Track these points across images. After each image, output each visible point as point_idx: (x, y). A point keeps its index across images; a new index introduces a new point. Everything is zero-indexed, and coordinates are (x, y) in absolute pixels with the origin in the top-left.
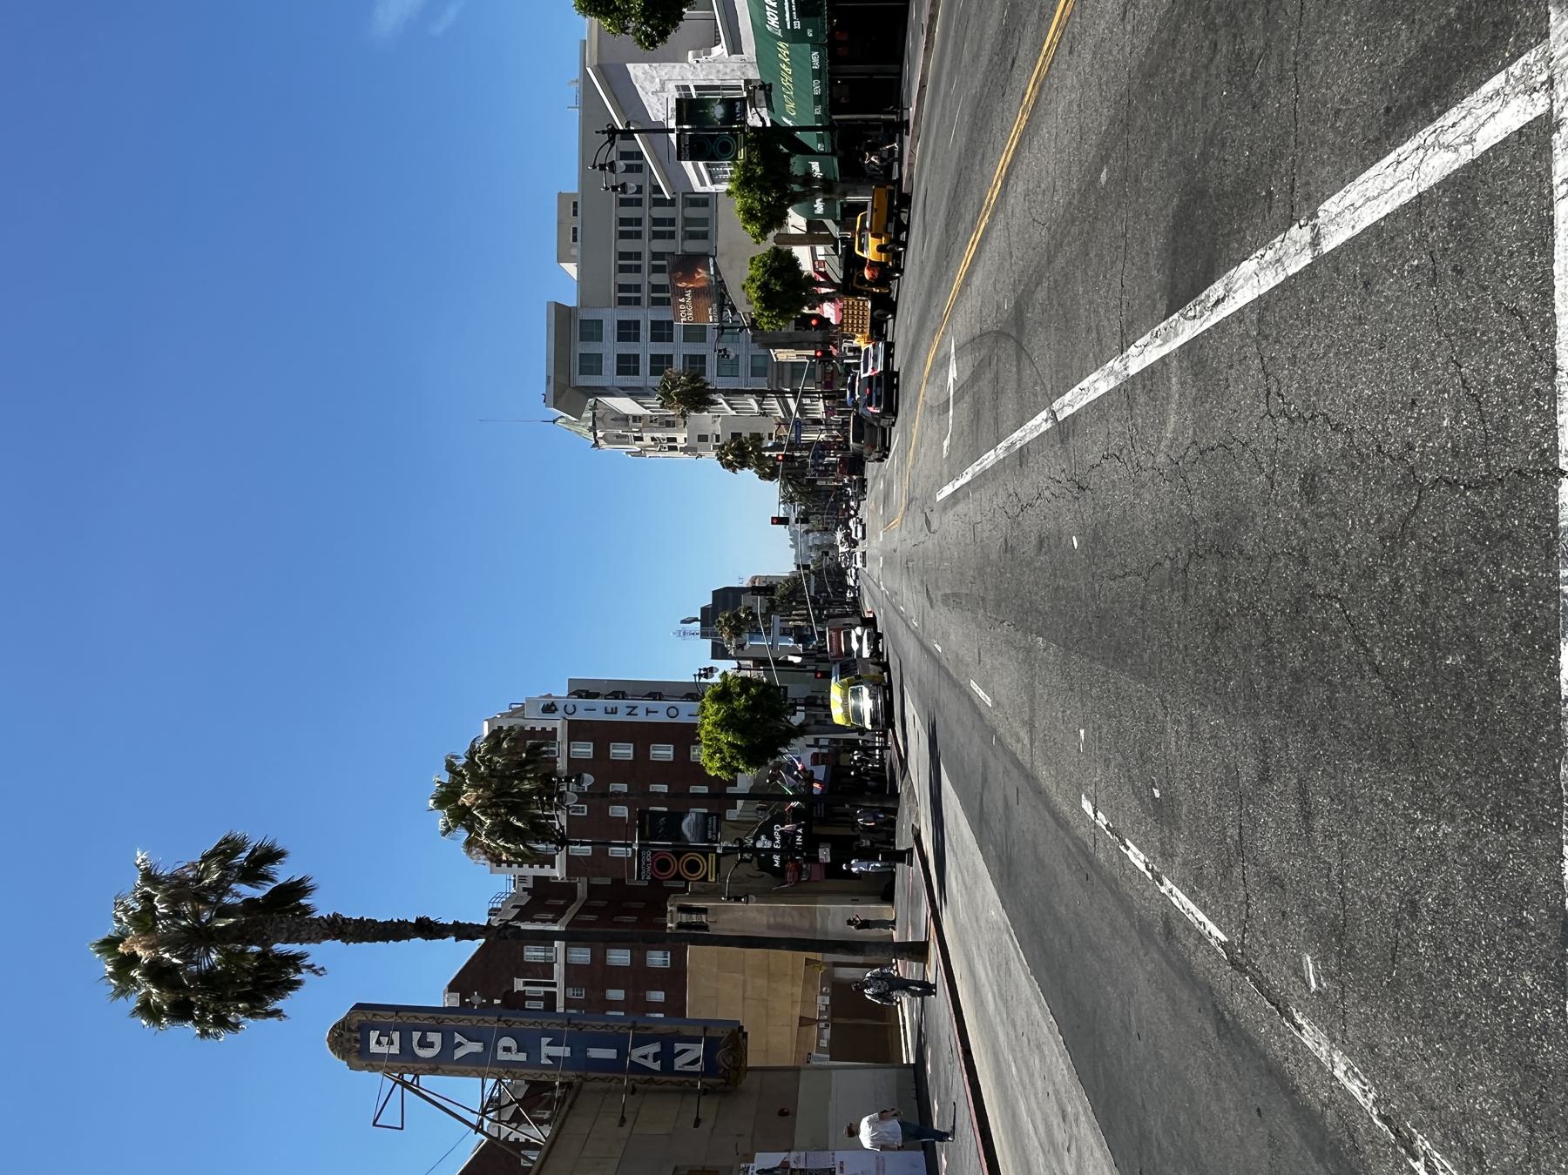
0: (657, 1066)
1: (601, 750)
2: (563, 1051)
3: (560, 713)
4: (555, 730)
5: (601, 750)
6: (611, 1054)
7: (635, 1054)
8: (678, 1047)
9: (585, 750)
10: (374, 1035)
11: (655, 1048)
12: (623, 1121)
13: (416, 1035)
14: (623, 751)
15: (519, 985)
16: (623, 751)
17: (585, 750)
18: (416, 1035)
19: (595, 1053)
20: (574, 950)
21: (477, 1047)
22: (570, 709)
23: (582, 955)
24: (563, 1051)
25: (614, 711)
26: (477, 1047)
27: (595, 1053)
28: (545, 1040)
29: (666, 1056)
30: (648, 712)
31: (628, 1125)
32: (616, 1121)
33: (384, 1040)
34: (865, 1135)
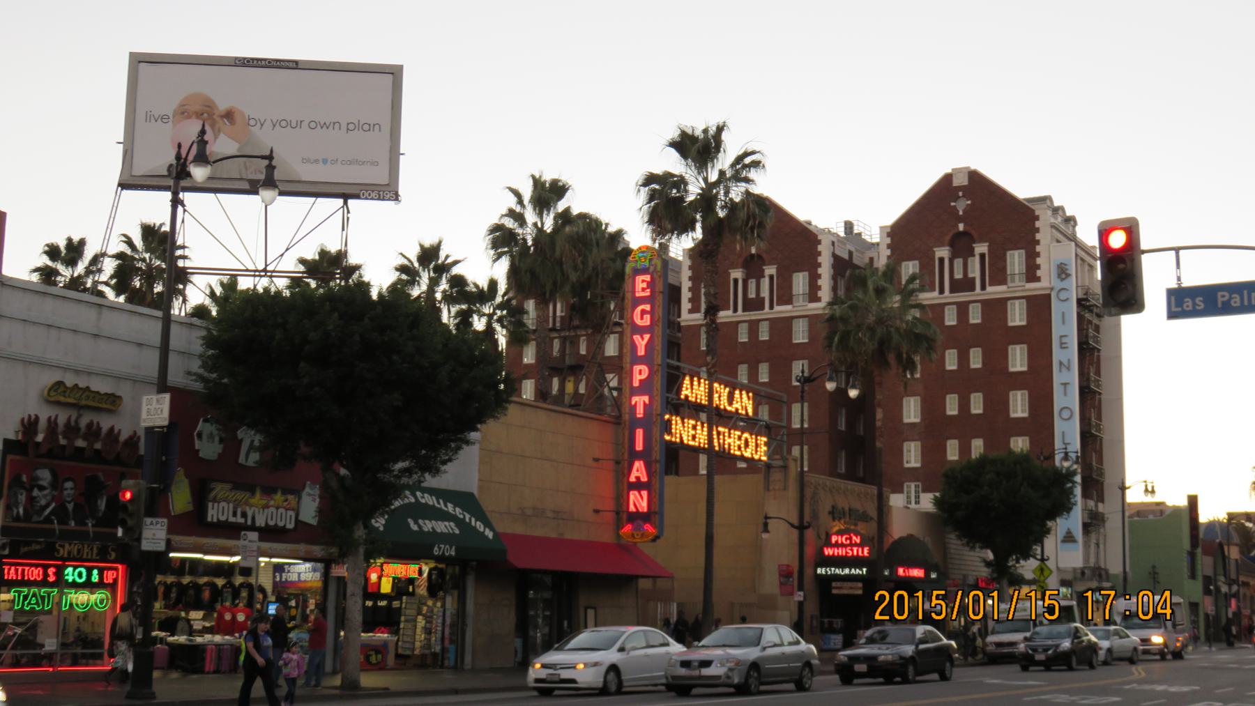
0: (632, 479)
1: (1017, 335)
2: (640, 412)
3: (1058, 284)
4: (1038, 279)
5: (1017, 335)
6: (639, 446)
7: (638, 465)
8: (644, 493)
9: (1017, 316)
10: (648, 278)
11: (644, 479)
12: (596, 460)
13: (648, 307)
14: (1018, 359)
15: (770, 270)
16: (1018, 359)
17: (1017, 316)
18: (648, 307)
19: (640, 433)
20: (806, 324)
21: (641, 352)
22: (1063, 295)
23: (800, 335)
24: (640, 412)
25: (1063, 346)
26: (641, 352)
27: (640, 433)
28: (646, 399)
29: (638, 486)
30: (1065, 384)
31: (595, 464)
32: (597, 456)
33: (645, 285)
34: (128, 495)
